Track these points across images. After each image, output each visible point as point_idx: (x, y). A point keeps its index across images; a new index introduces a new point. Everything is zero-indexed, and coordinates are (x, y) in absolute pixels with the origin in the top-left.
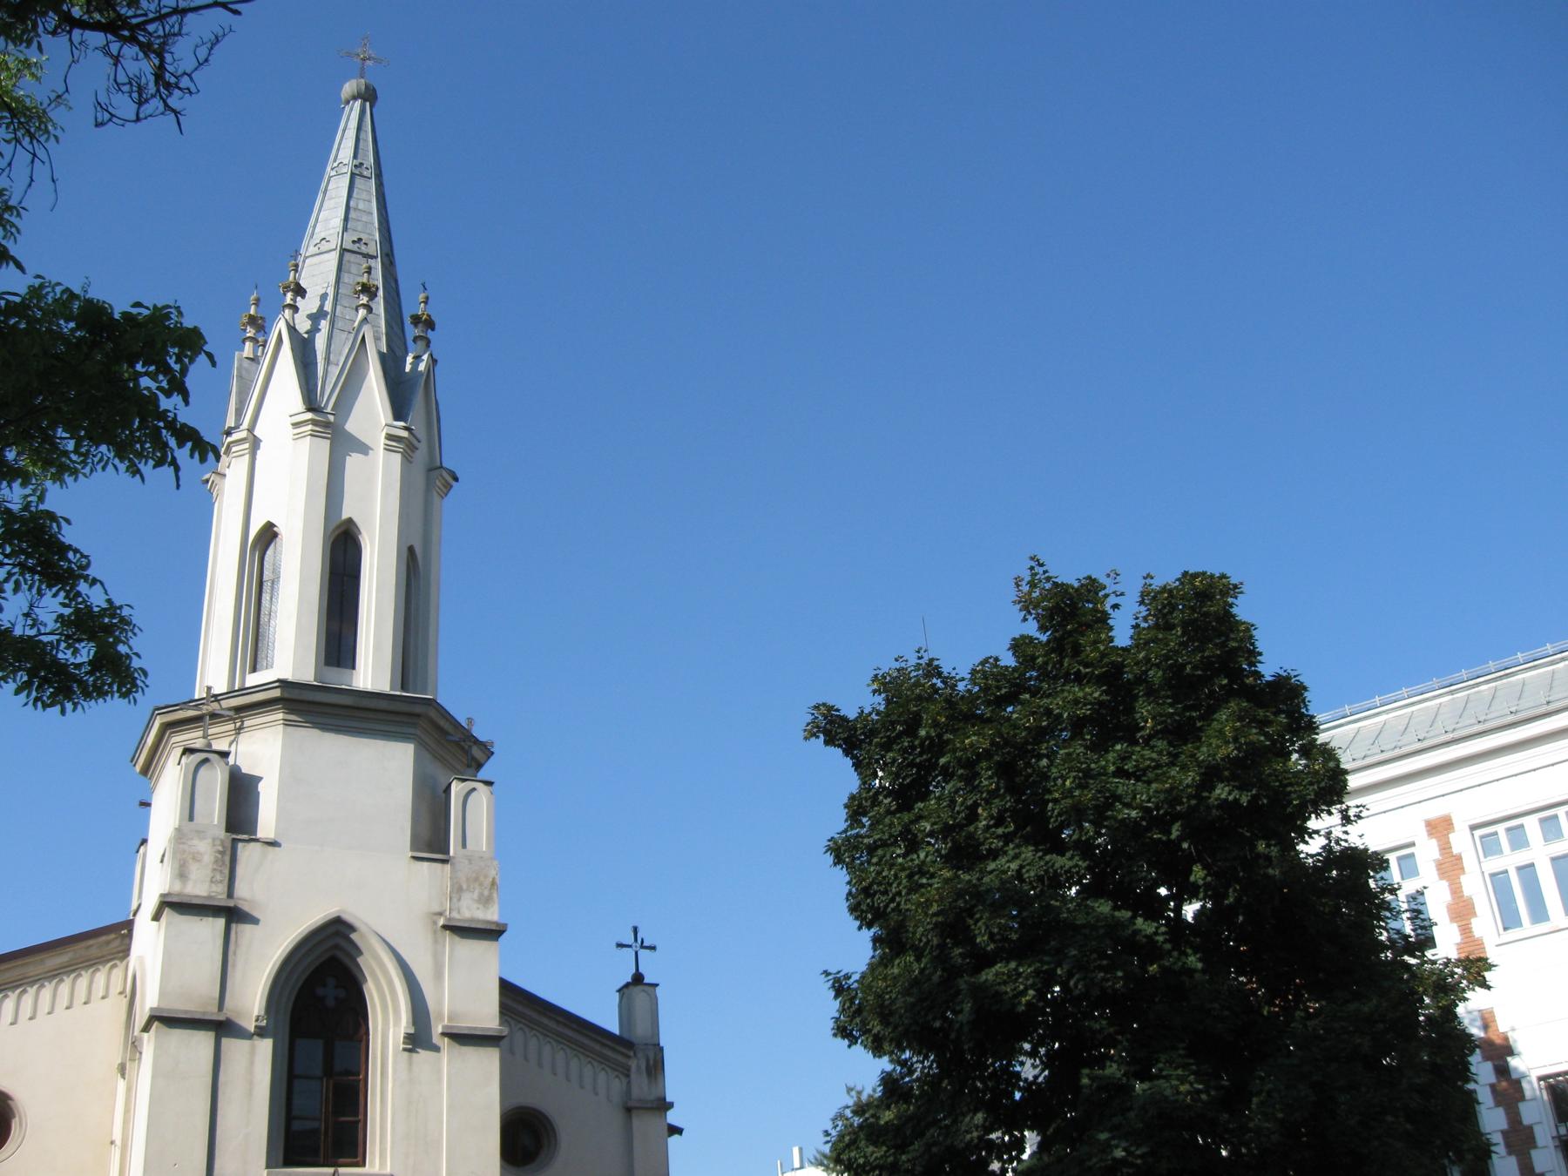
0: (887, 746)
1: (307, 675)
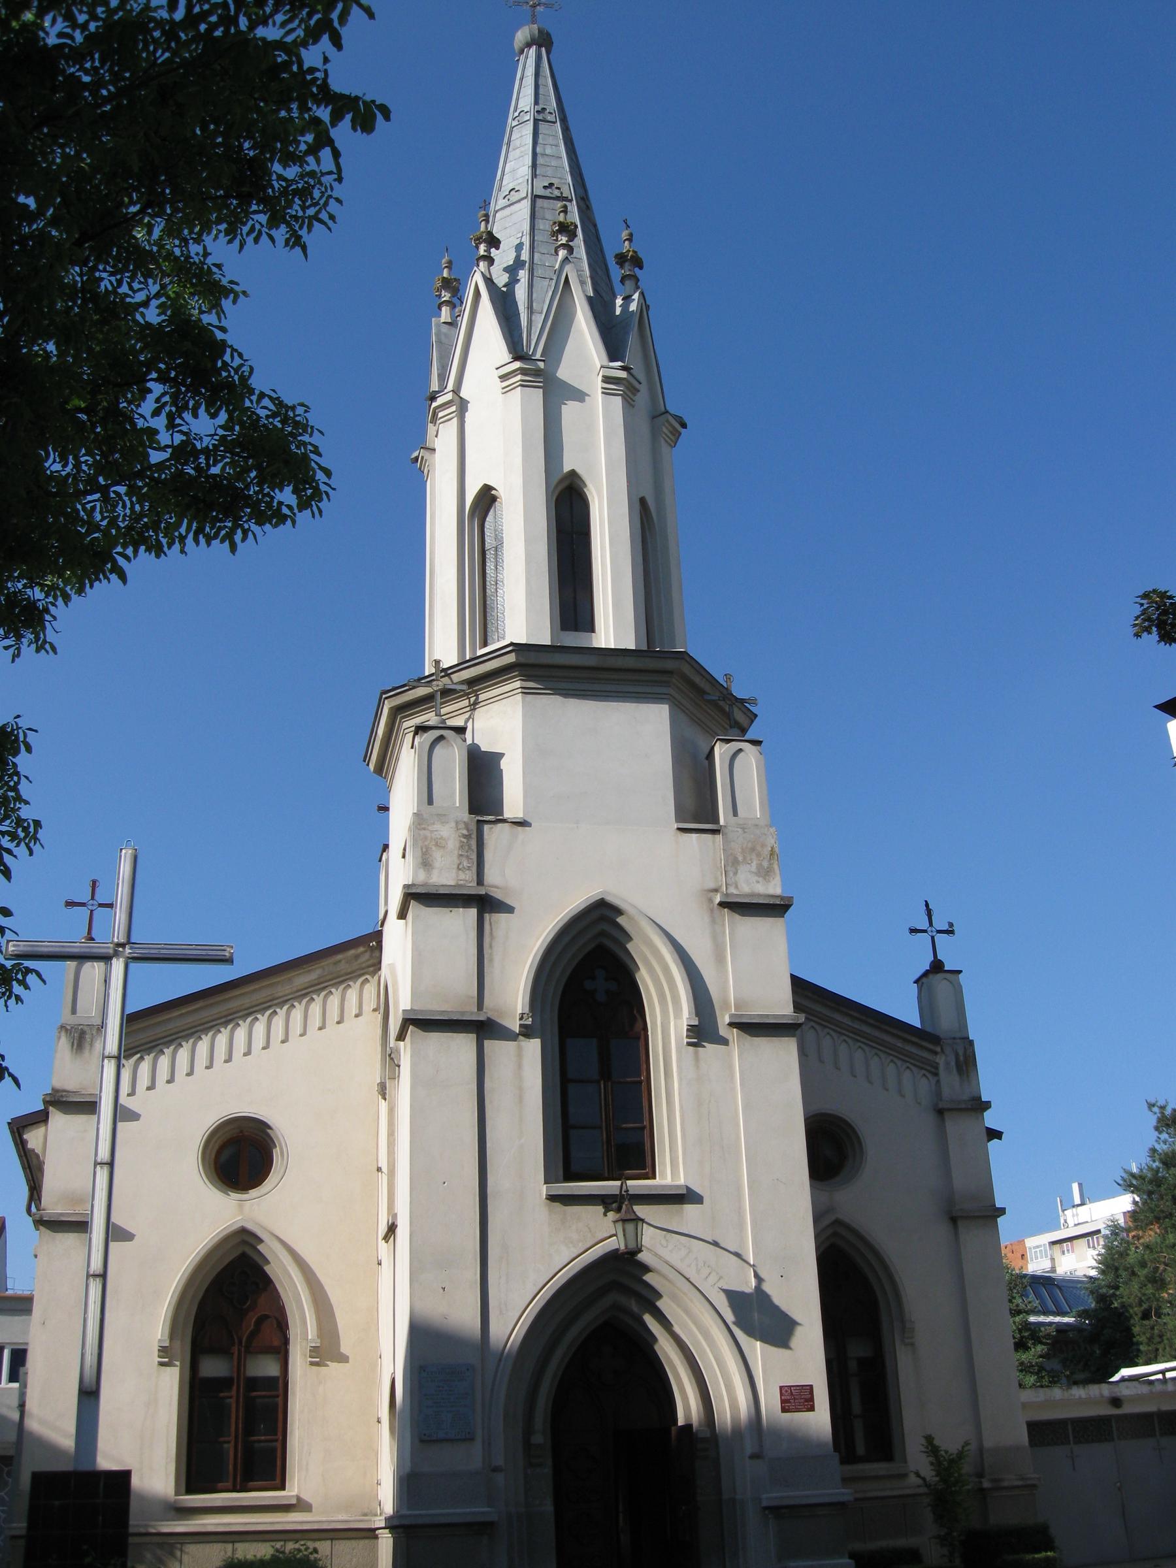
1: (544, 638)
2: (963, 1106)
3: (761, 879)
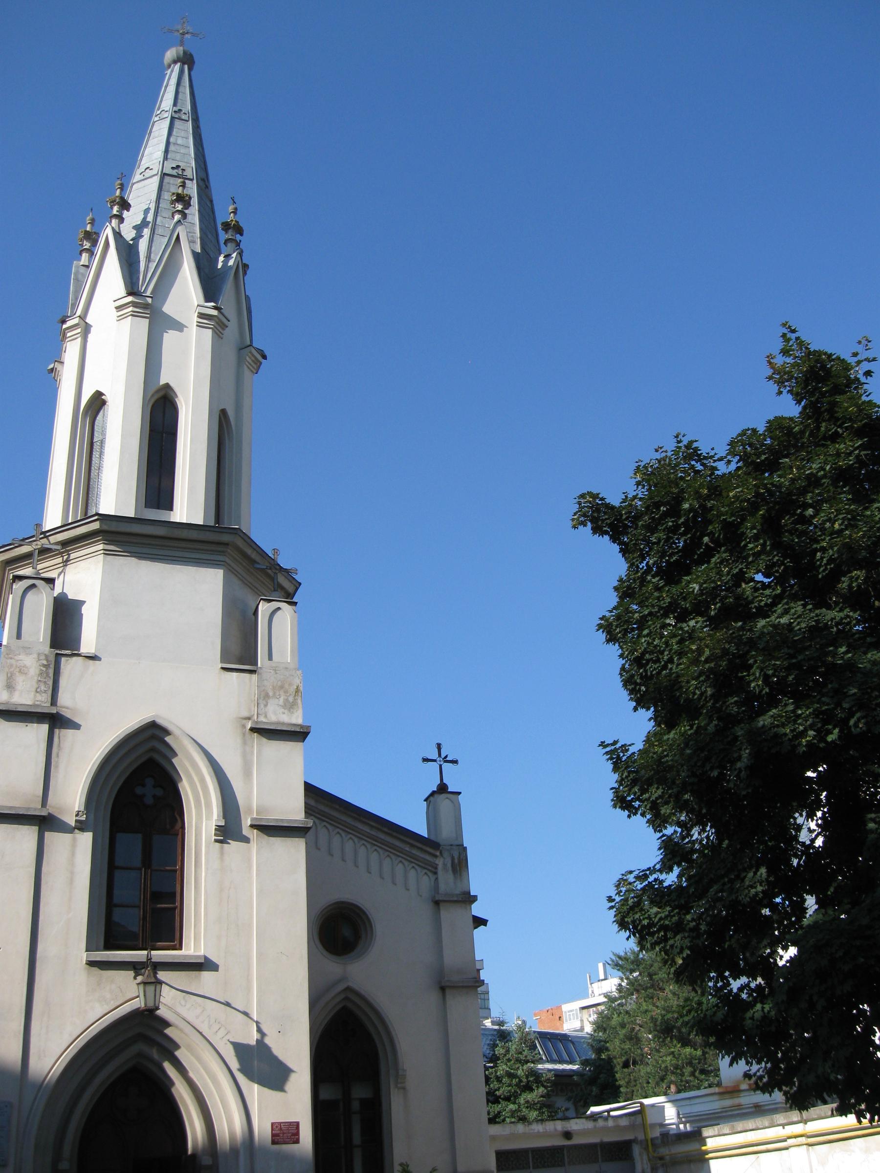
0: (651, 529)
2: (455, 899)
3: (286, 711)
